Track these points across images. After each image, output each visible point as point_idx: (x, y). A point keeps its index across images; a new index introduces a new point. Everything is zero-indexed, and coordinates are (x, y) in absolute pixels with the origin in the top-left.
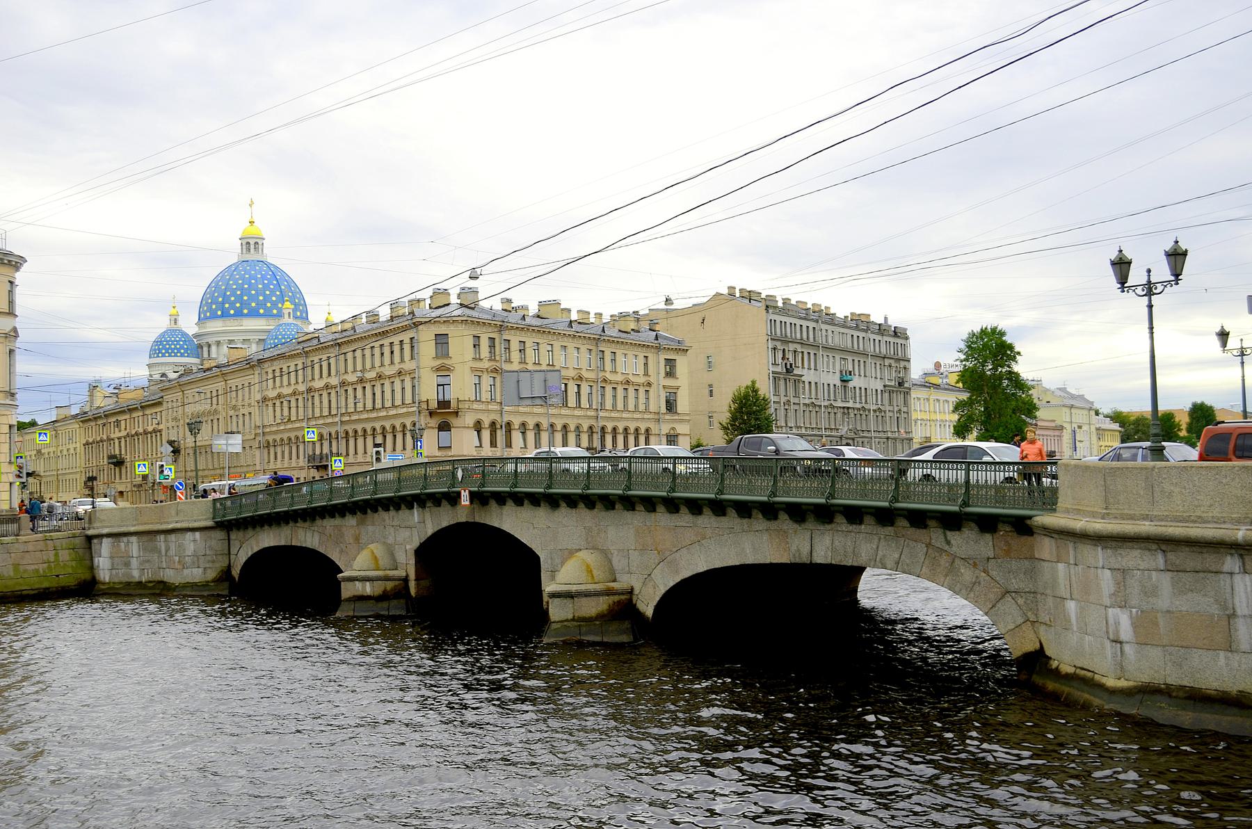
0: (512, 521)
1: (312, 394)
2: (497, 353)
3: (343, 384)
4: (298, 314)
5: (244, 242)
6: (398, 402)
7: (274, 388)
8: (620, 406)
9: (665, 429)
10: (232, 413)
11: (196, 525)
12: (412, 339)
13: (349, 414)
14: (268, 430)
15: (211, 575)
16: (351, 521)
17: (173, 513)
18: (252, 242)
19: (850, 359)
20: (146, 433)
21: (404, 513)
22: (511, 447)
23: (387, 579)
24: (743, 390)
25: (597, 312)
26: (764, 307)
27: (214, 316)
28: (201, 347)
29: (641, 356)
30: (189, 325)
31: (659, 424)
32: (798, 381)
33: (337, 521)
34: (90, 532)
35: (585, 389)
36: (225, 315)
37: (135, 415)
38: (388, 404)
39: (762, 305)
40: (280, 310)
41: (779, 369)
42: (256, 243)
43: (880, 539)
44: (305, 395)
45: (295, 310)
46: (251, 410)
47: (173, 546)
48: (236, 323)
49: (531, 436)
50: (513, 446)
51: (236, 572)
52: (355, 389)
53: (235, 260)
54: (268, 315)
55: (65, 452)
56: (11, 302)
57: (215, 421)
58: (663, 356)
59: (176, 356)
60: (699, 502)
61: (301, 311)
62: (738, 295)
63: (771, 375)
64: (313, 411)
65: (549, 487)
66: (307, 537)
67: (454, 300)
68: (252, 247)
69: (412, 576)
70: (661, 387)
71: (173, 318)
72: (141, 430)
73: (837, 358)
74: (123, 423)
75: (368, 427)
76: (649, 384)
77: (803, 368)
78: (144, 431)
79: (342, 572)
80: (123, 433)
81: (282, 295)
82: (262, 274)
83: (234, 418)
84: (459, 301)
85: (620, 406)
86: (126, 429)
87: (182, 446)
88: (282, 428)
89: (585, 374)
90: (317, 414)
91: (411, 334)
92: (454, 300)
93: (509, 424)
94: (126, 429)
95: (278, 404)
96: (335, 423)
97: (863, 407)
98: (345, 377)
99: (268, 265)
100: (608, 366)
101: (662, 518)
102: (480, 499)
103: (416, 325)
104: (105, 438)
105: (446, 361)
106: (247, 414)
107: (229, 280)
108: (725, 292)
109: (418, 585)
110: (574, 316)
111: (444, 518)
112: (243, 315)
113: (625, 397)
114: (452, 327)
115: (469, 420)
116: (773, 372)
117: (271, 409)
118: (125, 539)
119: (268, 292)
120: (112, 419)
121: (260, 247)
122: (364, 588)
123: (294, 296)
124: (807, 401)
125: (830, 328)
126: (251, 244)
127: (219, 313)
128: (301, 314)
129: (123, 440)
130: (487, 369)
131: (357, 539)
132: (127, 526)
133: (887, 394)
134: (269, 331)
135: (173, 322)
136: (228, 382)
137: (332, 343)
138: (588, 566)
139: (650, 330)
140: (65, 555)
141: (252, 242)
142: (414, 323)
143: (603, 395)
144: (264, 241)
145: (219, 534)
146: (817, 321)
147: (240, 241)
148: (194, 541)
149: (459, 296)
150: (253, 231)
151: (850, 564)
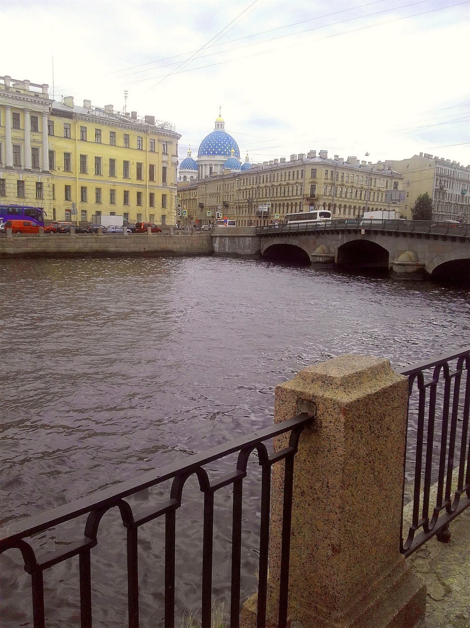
0: (379, 241)
2: (334, 177)
3: (272, 186)
6: (294, 194)
7: (244, 186)
8: (376, 200)
10: (226, 194)
11: (250, 235)
13: (274, 198)
15: (254, 252)
16: (313, 237)
17: (242, 230)
18: (220, 124)
19: (467, 184)
20: (190, 199)
21: (335, 236)
22: (335, 214)
23: (328, 257)
24: (422, 196)
27: (204, 154)
28: (199, 166)
29: (385, 180)
30: (195, 156)
32: (444, 193)
33: (307, 237)
34: (213, 235)
35: (363, 193)
36: (209, 153)
37: (186, 192)
38: (290, 195)
41: (438, 188)
42: (221, 124)
47: (241, 242)
49: (342, 210)
50: (336, 213)
51: (262, 252)
52: (277, 188)
53: (213, 131)
54: (225, 154)
59: (190, 169)
61: (237, 153)
62: (423, 156)
65: (413, 230)
66: (294, 242)
67: (317, 155)
68: (220, 126)
69: (336, 256)
71: (189, 154)
72: (188, 198)
73: (462, 184)
75: (282, 203)
77: (447, 187)
83: (227, 196)
84: (319, 156)
85: (376, 200)
86: (182, 197)
87: (205, 206)
89: (364, 187)
92: (317, 155)
93: (335, 205)
94: (182, 197)
95: (245, 192)
97: (456, 203)
98: (274, 183)
99: (226, 134)
100: (373, 184)
101: (440, 242)
102: (368, 232)
108: (419, 155)
109: (338, 261)
110: (361, 163)
111: (352, 238)
113: (378, 197)
115: (321, 203)
117: (242, 194)
118: (224, 238)
119: (225, 145)
122: (320, 259)
124: (447, 201)
125: (460, 171)
126: (219, 125)
127: (206, 152)
131: (315, 243)
132: (225, 234)
133: (438, 193)
134: (225, 161)
135: (189, 155)
138: (410, 256)
139: (389, 169)
140: (205, 242)
141: (220, 124)
143: (370, 195)
145: (257, 239)
146: (455, 168)
148: (249, 240)
149: (319, 154)
150: (220, 119)
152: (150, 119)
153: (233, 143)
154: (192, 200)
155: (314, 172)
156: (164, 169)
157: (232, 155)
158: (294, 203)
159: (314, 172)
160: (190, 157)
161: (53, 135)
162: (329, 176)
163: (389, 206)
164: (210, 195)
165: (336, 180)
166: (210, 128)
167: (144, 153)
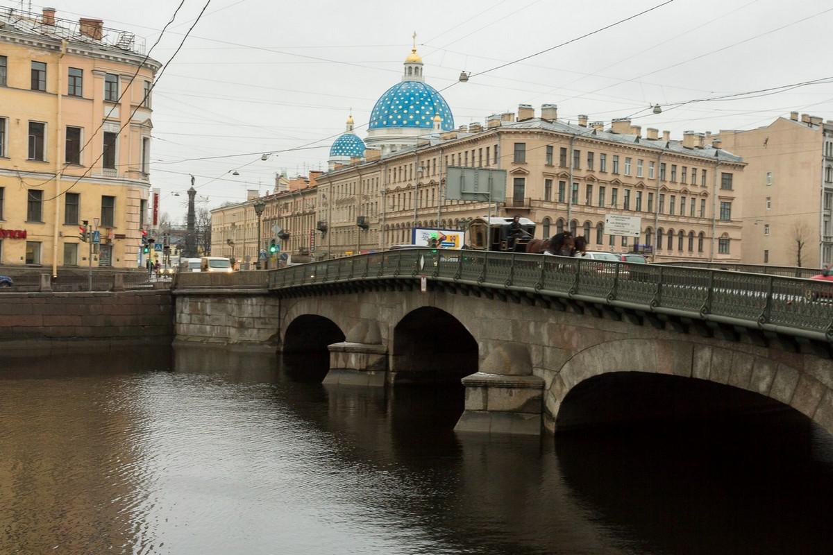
1: (421, 189)
4: (446, 126)
5: (407, 66)
8: (687, 213)
9: (718, 233)
10: (363, 201)
12: (496, 146)
13: (447, 207)
14: (388, 216)
18: (414, 66)
25: (665, 130)
26: (822, 131)
27: (381, 126)
31: (712, 229)
39: (819, 129)
40: (432, 122)
42: (417, 68)
43: (755, 360)
44: (416, 190)
45: (443, 123)
46: (378, 199)
48: (398, 131)
55: (250, 226)
56: (147, 97)
57: (352, 207)
58: (720, 171)
60: (616, 308)
63: (823, 191)
64: (427, 202)
65: (483, 280)
67: (538, 114)
68: (413, 71)
70: (716, 197)
74: (290, 205)
76: (706, 195)
78: (303, 212)
79: (343, 339)
80: (290, 214)
81: (435, 110)
82: (419, 93)
87: (328, 226)
88: (398, 215)
89: (646, 183)
90: (401, 209)
91: (495, 141)
92: (538, 114)
95: (396, 196)
96: (435, 214)
100: (668, 177)
103: (499, 134)
104: (277, 216)
105: (523, 167)
106: (374, 203)
107: (394, 96)
108: (788, 116)
112: (404, 126)
114: (529, 138)
116: (826, 189)
117: (391, 199)
120: (283, 202)
121: (420, 71)
123: (444, 112)
127: (385, 123)
128: (449, 126)
129: (289, 219)
130: (557, 174)
136: (363, 176)
137: (436, 147)
139: (713, 147)
141: (414, 66)
142: (498, 133)
144: (423, 67)
147: (404, 66)
150: (413, 57)
151: (725, 383)
152: (93, 27)
153: (440, 103)
154: (308, 214)
155: (519, 150)
156: (110, 138)
157: (436, 127)
158: (676, 232)
159: (519, 150)
160: (350, 133)
161: (81, 97)
162: (556, 159)
163: (712, 226)
164: (339, 202)
165: (572, 167)
166: (395, 77)
167: (51, 99)
